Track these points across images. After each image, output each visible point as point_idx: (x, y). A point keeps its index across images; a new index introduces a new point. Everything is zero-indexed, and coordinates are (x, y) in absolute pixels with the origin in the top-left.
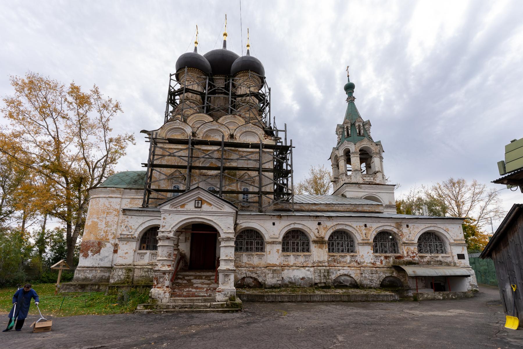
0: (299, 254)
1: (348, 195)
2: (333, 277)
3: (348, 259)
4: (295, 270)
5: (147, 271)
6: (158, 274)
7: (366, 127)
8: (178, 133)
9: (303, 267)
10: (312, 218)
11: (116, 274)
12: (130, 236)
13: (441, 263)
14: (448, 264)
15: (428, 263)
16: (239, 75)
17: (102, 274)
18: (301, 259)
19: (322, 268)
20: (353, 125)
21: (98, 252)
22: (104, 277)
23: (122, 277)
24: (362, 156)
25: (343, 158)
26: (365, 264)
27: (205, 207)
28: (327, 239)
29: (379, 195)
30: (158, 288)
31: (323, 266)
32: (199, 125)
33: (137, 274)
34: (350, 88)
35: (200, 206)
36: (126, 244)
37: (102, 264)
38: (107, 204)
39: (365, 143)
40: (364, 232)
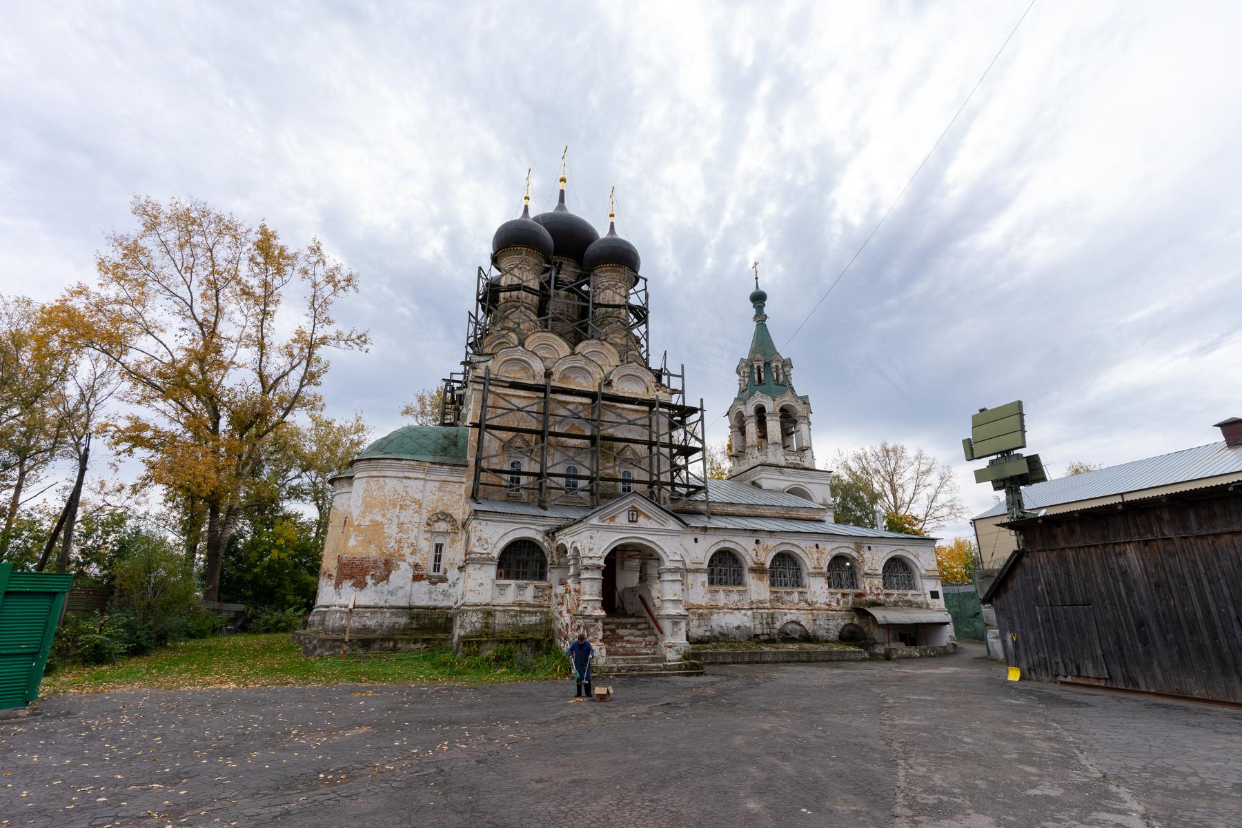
0: (731, 588)
1: (765, 484)
2: (778, 625)
3: (796, 596)
7: (786, 369)
8: (517, 368)
10: (748, 534)
13: (910, 604)
14: (919, 606)
15: (896, 604)
17: (394, 619)
18: (735, 597)
20: (767, 364)
21: (386, 578)
23: (478, 626)
27: (642, 521)
28: (768, 565)
29: (809, 486)
32: (544, 354)
33: (500, 620)
34: (759, 299)
38: (400, 490)
39: (786, 400)
40: (816, 556)
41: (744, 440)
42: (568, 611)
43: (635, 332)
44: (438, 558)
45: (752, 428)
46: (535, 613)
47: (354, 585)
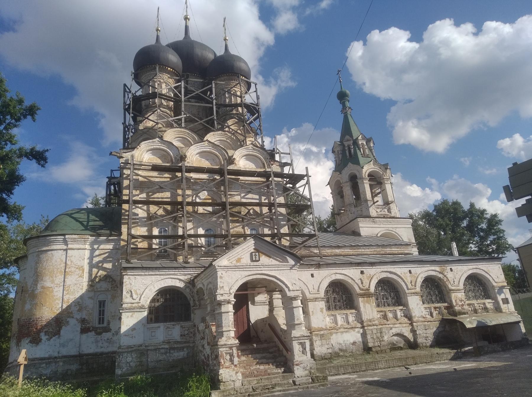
4: (345, 334)
5: (166, 353)
6: (224, 349)
16: (222, 78)
19: (372, 327)
21: (57, 333)
22: (69, 372)
24: (372, 183)
25: (348, 184)
26: (417, 318)
28: (372, 289)
30: (226, 368)
31: (374, 326)
33: (153, 357)
35: (257, 259)
36: (131, 316)
37: (64, 352)
41: (343, 202)
42: (208, 344)
44: (102, 313)
45: (347, 190)
46: (182, 349)
47: (30, 342)
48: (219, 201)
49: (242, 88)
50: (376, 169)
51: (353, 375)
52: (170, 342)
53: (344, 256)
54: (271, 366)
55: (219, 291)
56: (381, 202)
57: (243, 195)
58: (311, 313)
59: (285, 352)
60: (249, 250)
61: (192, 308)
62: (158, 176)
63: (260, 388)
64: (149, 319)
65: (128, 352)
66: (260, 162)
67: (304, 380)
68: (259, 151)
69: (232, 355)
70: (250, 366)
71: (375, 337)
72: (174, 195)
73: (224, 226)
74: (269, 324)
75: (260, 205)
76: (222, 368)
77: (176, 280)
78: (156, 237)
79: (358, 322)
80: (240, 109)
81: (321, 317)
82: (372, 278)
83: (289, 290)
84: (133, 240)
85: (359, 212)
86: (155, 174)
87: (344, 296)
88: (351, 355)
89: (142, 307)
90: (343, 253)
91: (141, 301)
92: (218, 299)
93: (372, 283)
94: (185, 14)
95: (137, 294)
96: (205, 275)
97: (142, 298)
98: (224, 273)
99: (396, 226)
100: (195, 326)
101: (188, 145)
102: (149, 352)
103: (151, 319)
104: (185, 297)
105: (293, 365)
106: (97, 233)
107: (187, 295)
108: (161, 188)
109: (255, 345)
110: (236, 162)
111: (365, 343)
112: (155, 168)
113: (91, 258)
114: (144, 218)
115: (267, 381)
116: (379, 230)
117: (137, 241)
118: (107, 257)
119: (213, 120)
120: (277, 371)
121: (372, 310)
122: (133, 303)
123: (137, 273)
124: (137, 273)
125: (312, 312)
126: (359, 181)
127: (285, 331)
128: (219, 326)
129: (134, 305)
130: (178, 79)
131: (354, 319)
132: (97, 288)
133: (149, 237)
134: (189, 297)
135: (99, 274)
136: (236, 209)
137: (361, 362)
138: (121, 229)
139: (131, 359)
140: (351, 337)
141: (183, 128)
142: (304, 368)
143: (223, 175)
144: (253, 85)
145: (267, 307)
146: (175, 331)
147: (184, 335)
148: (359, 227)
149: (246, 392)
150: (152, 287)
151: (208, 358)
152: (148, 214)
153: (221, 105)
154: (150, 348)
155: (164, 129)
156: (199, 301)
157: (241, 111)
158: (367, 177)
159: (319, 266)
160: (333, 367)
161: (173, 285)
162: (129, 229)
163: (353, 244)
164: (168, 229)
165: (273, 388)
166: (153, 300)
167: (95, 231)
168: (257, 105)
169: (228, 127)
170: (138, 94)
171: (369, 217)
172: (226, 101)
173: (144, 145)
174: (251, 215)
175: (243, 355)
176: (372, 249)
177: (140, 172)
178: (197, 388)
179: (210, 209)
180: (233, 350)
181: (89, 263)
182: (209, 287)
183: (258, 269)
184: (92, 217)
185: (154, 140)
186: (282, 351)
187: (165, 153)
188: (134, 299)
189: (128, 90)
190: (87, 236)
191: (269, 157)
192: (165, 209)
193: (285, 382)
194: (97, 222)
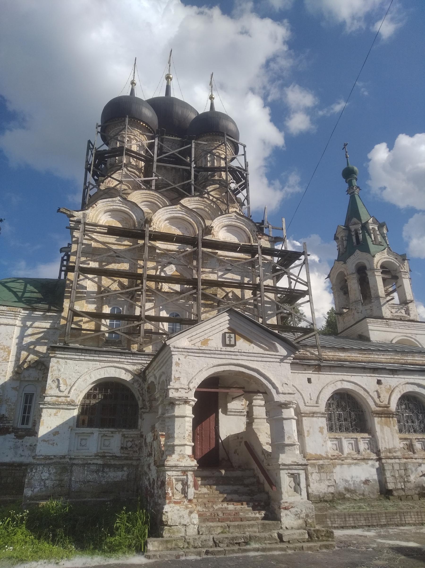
4: (353, 467)
6: (174, 473)
9: (364, 459)
11: (36, 477)
12: (63, 399)
16: (204, 138)
19: (393, 461)
25: (355, 276)
28: (393, 407)
30: (175, 503)
31: (395, 458)
33: (78, 476)
36: (55, 415)
43: (239, 196)
45: (354, 285)
46: (120, 467)
48: (189, 277)
49: (227, 150)
50: (392, 259)
51: (368, 531)
52: (105, 456)
53: (350, 362)
54: (245, 506)
55: (173, 384)
56: (396, 300)
57: (220, 273)
58: (306, 434)
59: (267, 486)
60: (221, 328)
61: (140, 411)
62: (116, 242)
63: (226, 541)
64: (81, 422)
65: (44, 465)
66: (244, 235)
67: (297, 534)
68: (244, 221)
69: (185, 484)
70: (214, 503)
71: (397, 475)
72: (134, 265)
73: (194, 310)
74: (246, 443)
75: (241, 286)
76: (169, 503)
77: (121, 369)
78: (106, 316)
79: (372, 451)
80: (223, 174)
81: (319, 440)
82: (392, 391)
83: (278, 393)
84: (76, 319)
85: (369, 311)
86: (111, 239)
87: (353, 413)
88: (361, 499)
89: (71, 404)
90: (349, 359)
91: (70, 395)
92: (171, 395)
93: (392, 398)
94: (168, 73)
95: (66, 384)
96: (157, 363)
97: (72, 391)
98: (182, 357)
99: (416, 332)
100: (142, 436)
101: (155, 208)
102: (74, 468)
103: (84, 421)
104: (132, 395)
105: (280, 508)
106: (32, 306)
107: (134, 392)
108: (117, 257)
109: (223, 472)
110: (214, 231)
111: (382, 482)
112: (111, 231)
113: (21, 337)
114: (93, 292)
115: (237, 530)
116: (394, 335)
117: (81, 321)
118: (41, 338)
119: (189, 184)
120: (253, 515)
121: (393, 435)
122: (60, 397)
123: (69, 356)
124: (69, 356)
125: (308, 431)
126: (369, 273)
127: (269, 454)
128: (170, 436)
129: (60, 399)
130: (151, 136)
131: (366, 447)
132: (24, 377)
133: (97, 316)
134: (137, 395)
135: (29, 359)
136: (210, 291)
137: (379, 511)
138: (63, 305)
139: (47, 475)
140: (364, 473)
141: (152, 190)
142: (296, 515)
143: (196, 244)
144: (241, 148)
145: (244, 420)
146: (115, 441)
147: (126, 448)
148: (368, 330)
149: (203, 547)
150: (88, 377)
151: (154, 484)
152: (99, 287)
153: (201, 168)
154: (75, 462)
155: (129, 191)
156: (150, 401)
157: (224, 178)
158: (379, 268)
159: (319, 368)
160: (337, 515)
161: (117, 376)
162: (72, 303)
163: (363, 348)
164: (123, 309)
165: (246, 543)
166: (88, 396)
167: (30, 304)
168: (246, 170)
169: (208, 193)
170: (102, 149)
171: (382, 318)
172: (207, 164)
173: (102, 205)
174: (230, 299)
175: (205, 485)
176: (388, 355)
177: (94, 236)
178: (128, 531)
179: (177, 287)
180: (187, 475)
181: (17, 344)
182: (161, 380)
183: (233, 357)
184: (30, 288)
185: (114, 199)
186: (263, 484)
187: (126, 216)
188: (60, 391)
189: (91, 147)
190: (19, 309)
191: (256, 230)
192: (121, 285)
193: (266, 534)
194: (35, 294)
